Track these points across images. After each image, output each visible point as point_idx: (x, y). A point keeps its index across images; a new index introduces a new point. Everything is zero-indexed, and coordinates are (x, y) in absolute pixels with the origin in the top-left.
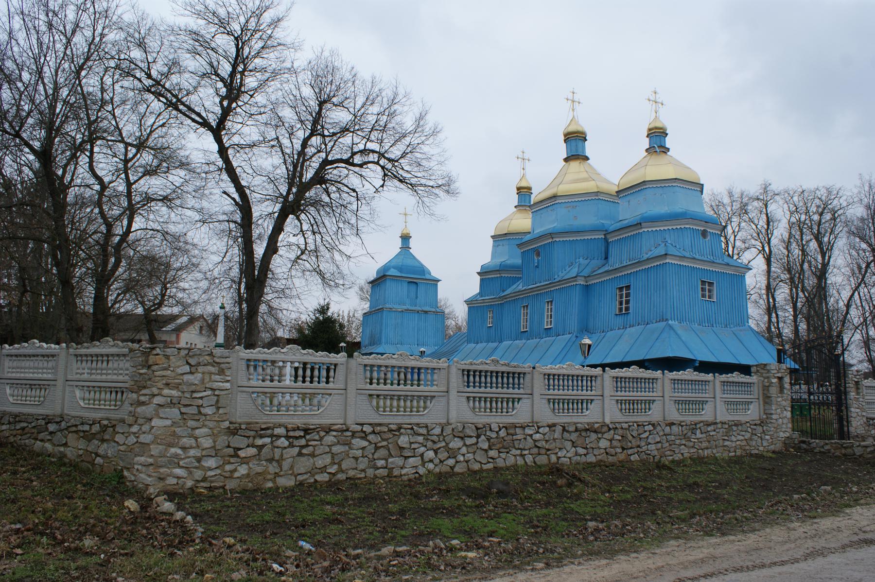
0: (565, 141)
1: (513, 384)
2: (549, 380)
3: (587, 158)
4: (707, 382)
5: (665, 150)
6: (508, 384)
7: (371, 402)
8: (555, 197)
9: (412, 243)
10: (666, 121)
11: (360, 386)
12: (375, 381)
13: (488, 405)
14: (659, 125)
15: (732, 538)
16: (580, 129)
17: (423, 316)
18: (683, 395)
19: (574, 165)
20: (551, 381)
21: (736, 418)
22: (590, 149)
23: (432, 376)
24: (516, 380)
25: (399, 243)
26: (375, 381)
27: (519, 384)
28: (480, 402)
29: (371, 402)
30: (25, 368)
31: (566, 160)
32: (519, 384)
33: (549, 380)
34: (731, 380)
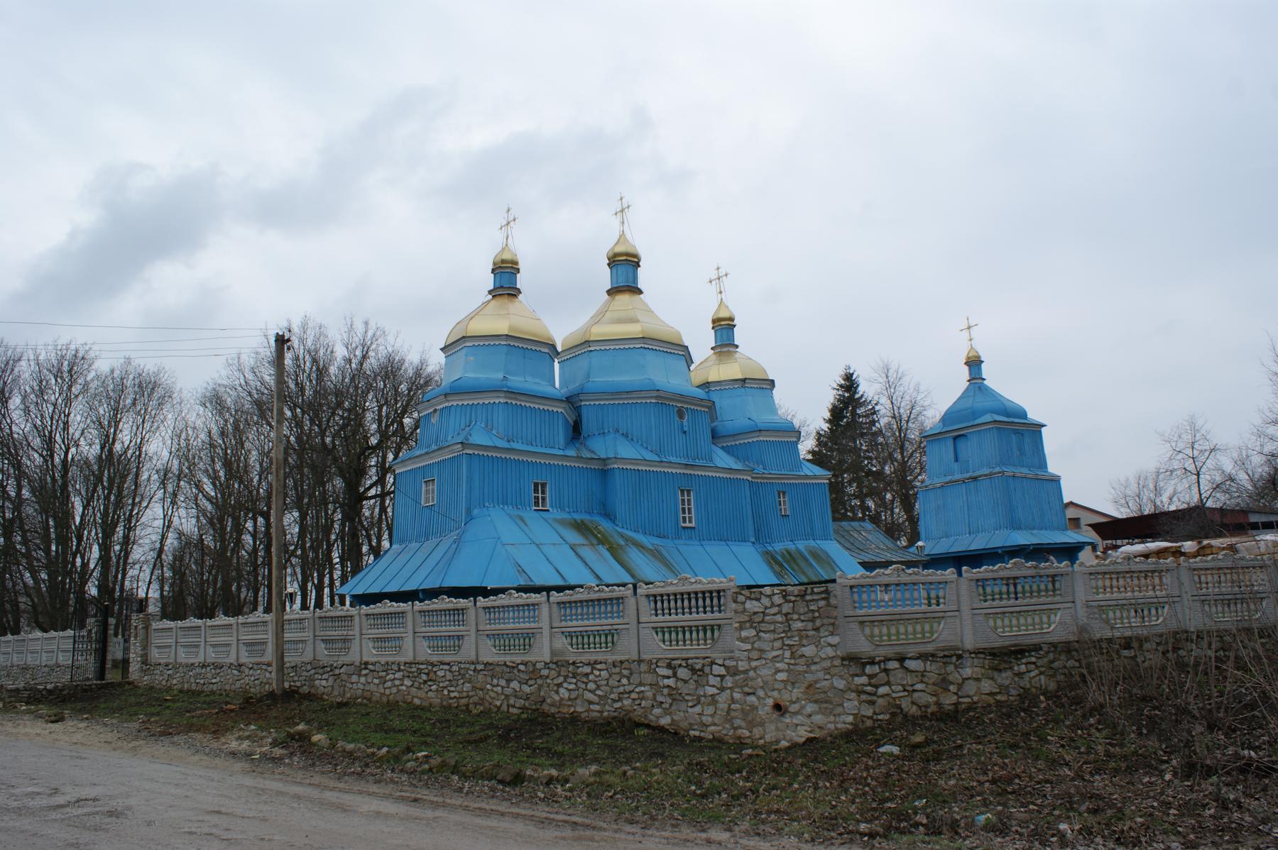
0: (493, 271)
1: (705, 607)
2: (656, 602)
3: (640, 292)
4: (462, 611)
5: (513, 293)
6: (705, 607)
7: (863, 631)
8: (587, 343)
9: (986, 370)
10: (526, 253)
11: (975, 606)
12: (933, 601)
13: (680, 636)
14: (507, 256)
15: (503, 807)
16: (630, 250)
17: (972, 485)
18: (522, 625)
19: (624, 299)
20: (659, 604)
21: (508, 659)
22: (644, 277)
23: (860, 596)
24: (715, 601)
25: (965, 372)
26: (933, 601)
27: (720, 606)
28: (670, 633)
29: (863, 631)
30: (116, 577)
31: (609, 292)
32: (720, 606)
33: (656, 602)
34: (376, 611)
